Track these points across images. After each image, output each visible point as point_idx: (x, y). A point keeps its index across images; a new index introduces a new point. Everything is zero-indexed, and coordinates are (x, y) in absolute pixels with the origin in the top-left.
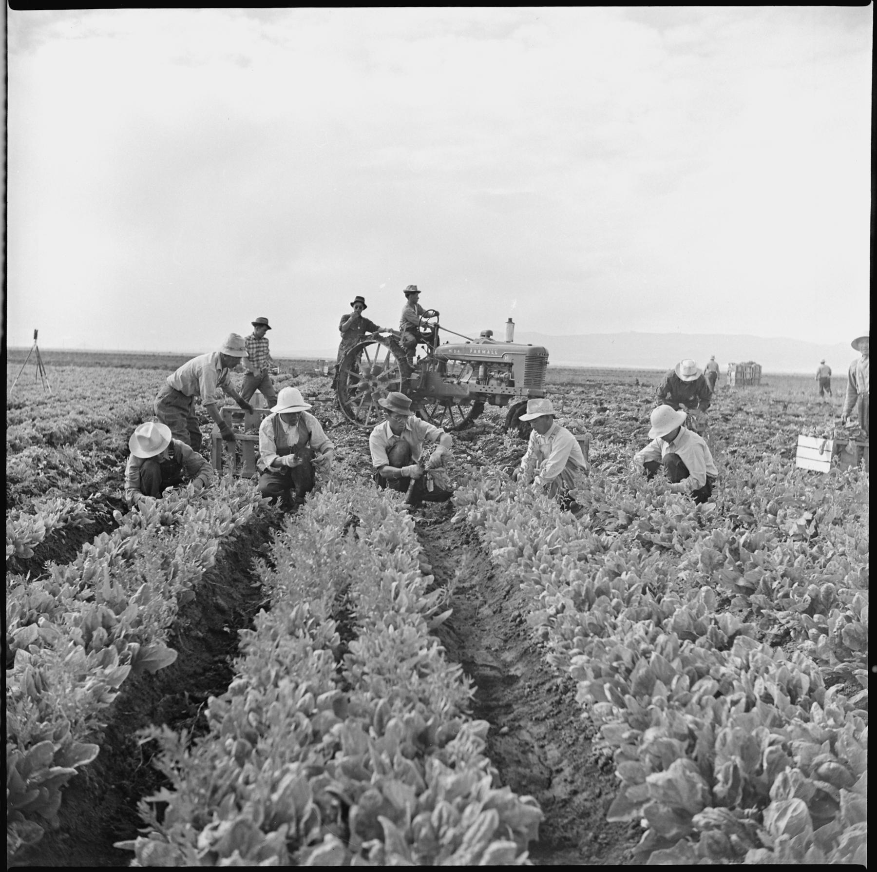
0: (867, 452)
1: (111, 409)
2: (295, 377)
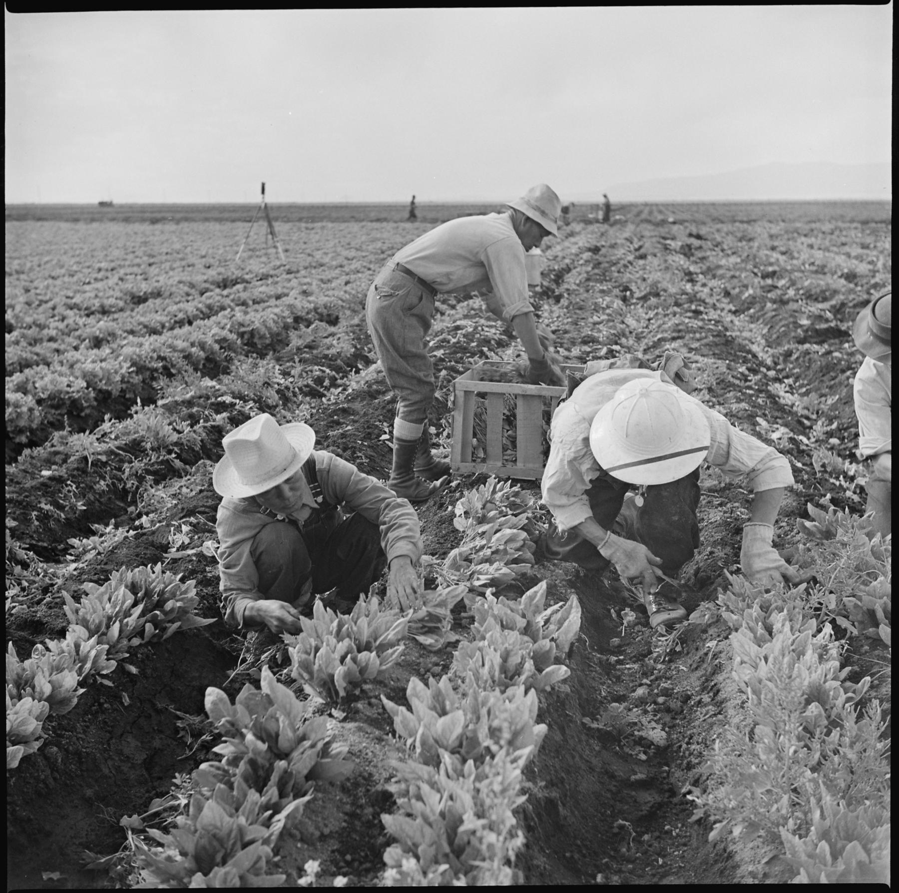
0: (877, 709)
1: (347, 283)
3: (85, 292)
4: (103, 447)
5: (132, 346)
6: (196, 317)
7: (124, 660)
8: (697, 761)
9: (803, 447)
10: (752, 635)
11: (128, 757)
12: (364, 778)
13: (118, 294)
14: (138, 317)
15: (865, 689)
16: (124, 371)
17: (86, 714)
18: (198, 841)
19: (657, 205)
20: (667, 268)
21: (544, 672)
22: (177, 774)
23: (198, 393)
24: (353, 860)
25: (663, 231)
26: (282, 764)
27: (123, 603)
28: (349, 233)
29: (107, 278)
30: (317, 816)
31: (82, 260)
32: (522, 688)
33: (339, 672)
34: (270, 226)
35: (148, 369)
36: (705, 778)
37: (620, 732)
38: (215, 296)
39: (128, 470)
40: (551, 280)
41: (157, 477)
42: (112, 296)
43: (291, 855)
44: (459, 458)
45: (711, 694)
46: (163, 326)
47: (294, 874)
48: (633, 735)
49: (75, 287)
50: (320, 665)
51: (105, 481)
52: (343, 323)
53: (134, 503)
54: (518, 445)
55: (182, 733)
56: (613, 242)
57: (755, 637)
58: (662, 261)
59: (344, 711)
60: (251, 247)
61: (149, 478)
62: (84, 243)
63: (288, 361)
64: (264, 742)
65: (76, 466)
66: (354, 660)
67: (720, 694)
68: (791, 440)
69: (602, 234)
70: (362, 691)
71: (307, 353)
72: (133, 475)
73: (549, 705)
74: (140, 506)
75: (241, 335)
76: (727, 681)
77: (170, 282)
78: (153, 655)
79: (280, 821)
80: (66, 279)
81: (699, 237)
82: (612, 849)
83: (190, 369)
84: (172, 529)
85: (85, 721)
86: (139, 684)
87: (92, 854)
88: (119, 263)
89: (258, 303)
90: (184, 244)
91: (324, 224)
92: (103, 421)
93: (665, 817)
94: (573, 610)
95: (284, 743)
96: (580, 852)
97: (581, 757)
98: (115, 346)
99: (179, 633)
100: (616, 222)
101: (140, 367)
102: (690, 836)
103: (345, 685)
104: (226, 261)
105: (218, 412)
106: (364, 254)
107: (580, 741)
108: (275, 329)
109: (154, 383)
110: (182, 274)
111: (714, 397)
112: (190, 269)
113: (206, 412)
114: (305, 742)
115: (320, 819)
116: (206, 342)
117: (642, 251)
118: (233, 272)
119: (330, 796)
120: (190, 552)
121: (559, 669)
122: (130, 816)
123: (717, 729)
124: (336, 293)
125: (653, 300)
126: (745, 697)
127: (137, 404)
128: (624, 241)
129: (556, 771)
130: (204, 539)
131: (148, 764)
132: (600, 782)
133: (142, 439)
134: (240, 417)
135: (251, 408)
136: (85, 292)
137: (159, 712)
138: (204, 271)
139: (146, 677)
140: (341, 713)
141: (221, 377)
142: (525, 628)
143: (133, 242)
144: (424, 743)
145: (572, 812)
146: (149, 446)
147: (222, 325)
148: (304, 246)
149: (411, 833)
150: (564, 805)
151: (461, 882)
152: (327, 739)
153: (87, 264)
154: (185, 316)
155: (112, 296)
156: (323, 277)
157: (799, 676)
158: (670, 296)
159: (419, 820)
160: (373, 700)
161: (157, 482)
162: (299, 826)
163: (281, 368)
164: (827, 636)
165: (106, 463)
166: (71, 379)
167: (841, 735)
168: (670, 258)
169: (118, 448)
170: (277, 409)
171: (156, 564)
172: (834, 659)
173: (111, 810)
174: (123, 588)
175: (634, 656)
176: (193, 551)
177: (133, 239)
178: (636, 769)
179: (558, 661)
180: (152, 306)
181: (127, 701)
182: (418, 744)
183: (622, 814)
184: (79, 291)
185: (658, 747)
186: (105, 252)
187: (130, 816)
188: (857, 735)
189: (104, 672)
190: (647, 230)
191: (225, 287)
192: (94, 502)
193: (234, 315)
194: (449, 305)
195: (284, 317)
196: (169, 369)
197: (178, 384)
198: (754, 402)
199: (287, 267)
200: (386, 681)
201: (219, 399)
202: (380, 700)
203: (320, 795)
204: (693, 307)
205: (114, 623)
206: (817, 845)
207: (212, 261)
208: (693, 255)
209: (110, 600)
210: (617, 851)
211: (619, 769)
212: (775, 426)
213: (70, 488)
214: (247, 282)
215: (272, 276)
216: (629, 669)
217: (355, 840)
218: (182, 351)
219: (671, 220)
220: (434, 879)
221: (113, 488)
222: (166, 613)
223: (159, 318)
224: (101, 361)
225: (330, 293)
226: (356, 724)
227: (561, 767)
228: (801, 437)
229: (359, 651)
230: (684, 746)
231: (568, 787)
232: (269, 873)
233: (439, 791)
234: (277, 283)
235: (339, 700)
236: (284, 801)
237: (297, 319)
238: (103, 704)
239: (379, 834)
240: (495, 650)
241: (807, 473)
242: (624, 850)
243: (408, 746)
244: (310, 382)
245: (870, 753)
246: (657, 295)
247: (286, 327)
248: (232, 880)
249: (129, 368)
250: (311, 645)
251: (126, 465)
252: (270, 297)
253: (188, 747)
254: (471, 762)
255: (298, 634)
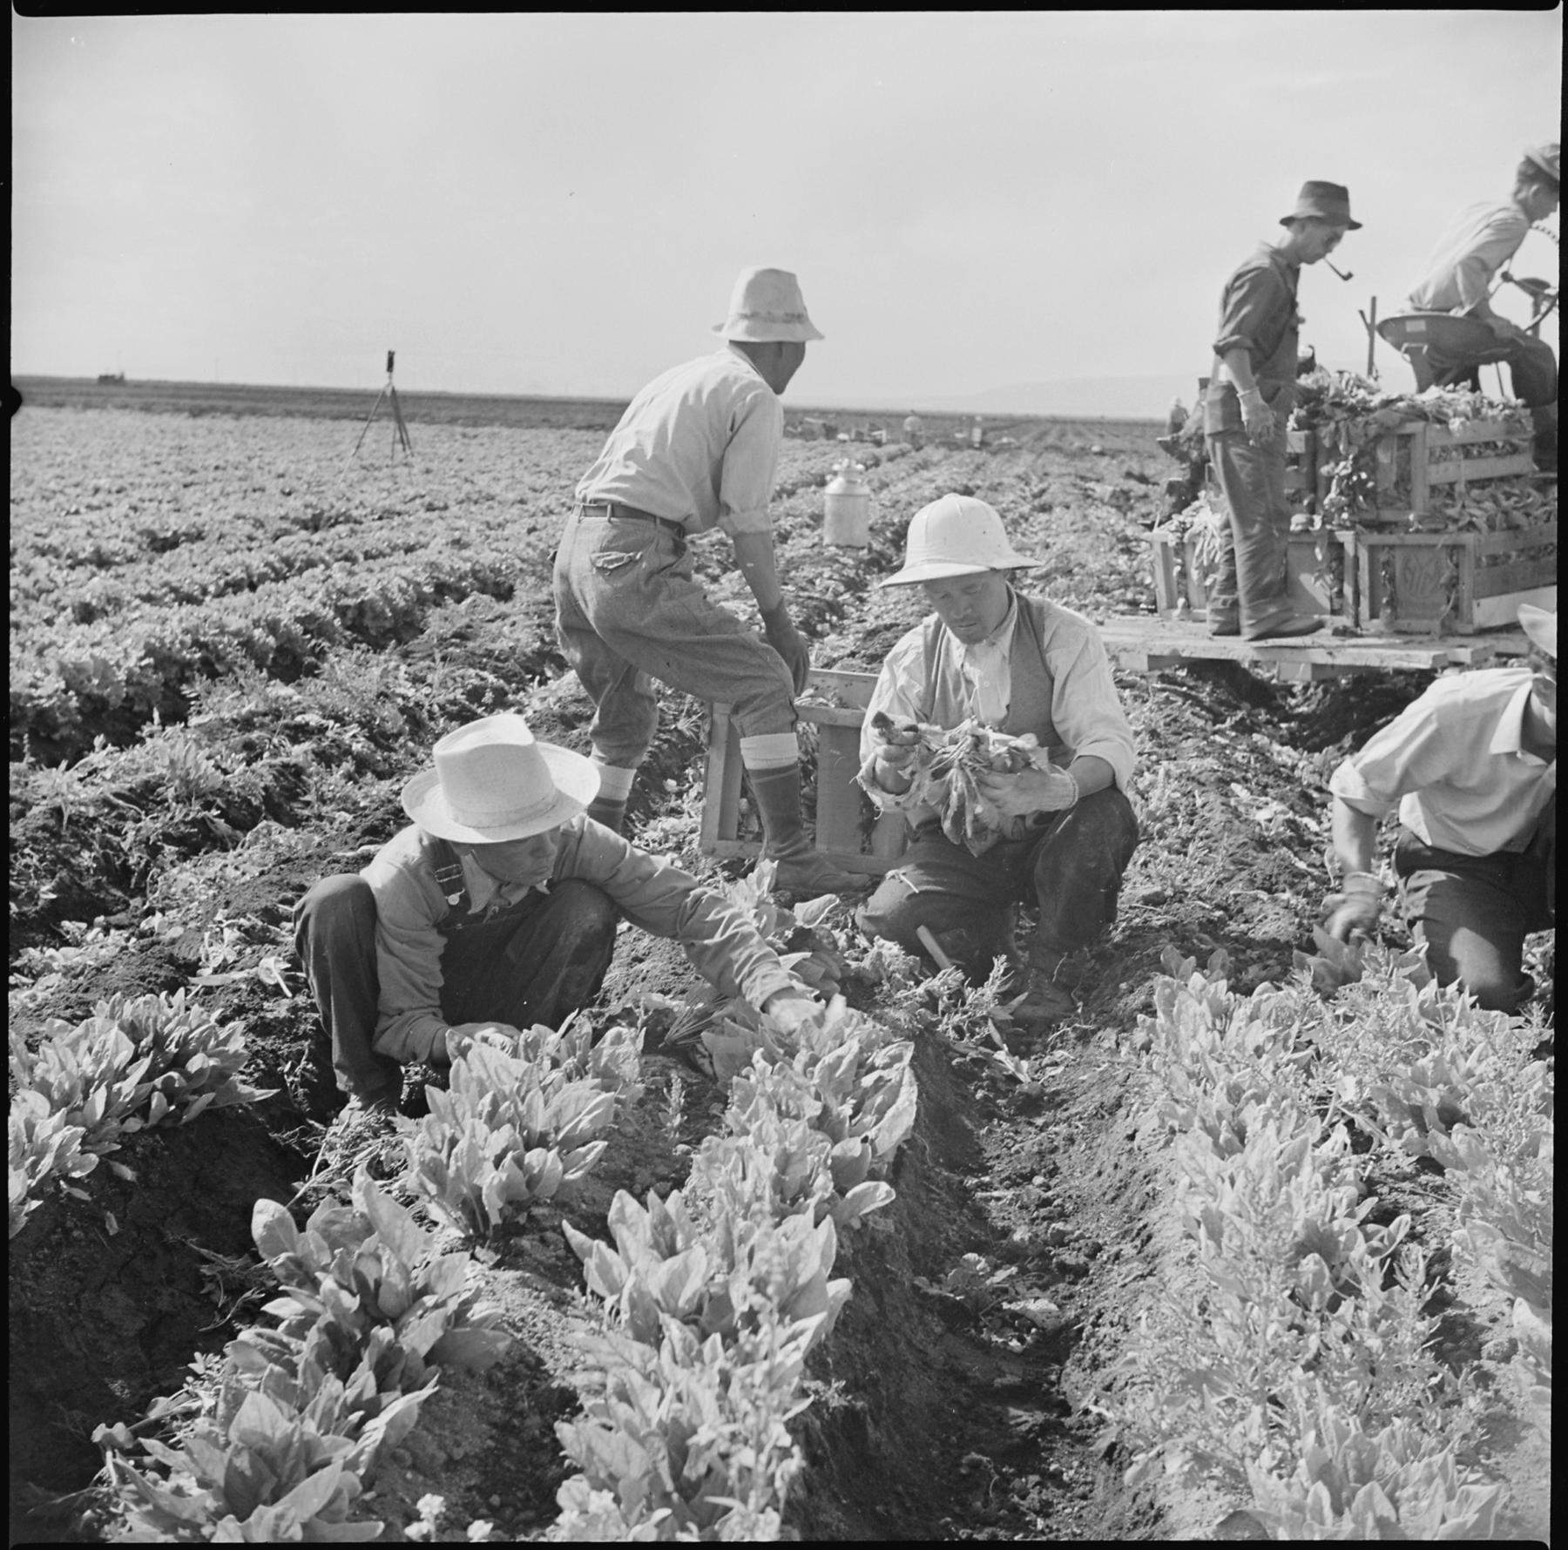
1: (531, 530)
2: (918, 450)
3: (68, 527)
4: (89, 793)
5: (150, 622)
6: (263, 578)
7: (111, 1155)
8: (1109, 1354)
9: (1308, 837)
10: (1210, 1139)
11: (111, 1325)
12: (528, 1366)
13: (129, 533)
14: (162, 572)
15: (1400, 1237)
16: (132, 663)
17: (40, 1246)
18: (230, 1461)
19: (1073, 422)
20: (1087, 529)
21: (849, 1195)
22: (197, 1355)
23: (262, 708)
24: (503, 1505)
25: (1083, 466)
26: (384, 1334)
27: (116, 1054)
28: (539, 446)
29: (109, 505)
30: (443, 1428)
31: (66, 473)
32: (810, 1214)
33: (490, 1180)
34: (402, 429)
35: (175, 662)
36: (1122, 1383)
37: (978, 1304)
38: (297, 544)
39: (131, 834)
40: (886, 540)
41: (183, 849)
42: (117, 536)
43: (394, 1491)
44: (716, 831)
45: (1138, 1242)
46: (205, 592)
47: (399, 1523)
48: (1000, 1309)
49: (50, 519)
50: (458, 1169)
51: (91, 851)
52: (522, 595)
53: (140, 891)
54: (819, 813)
55: (209, 1287)
56: (996, 481)
57: (1216, 1144)
58: (1079, 518)
59: (496, 1251)
60: (366, 463)
61: (168, 849)
62: (71, 443)
63: (423, 659)
64: (354, 1295)
65: (40, 823)
66: (519, 1161)
67: (1153, 1241)
68: (1291, 824)
69: (978, 468)
70: (531, 1218)
71: (457, 646)
72: (141, 842)
73: (856, 1252)
74: (151, 897)
75: (341, 611)
76: (1166, 1219)
77: (222, 515)
78: (164, 1149)
79: (376, 1430)
80: (37, 504)
81: (1143, 479)
82: (957, 1502)
83: (251, 666)
84: (207, 935)
85: (38, 1259)
86: (136, 1198)
87: (40, 1491)
88: (130, 479)
89: (374, 557)
90: (249, 453)
91: (496, 429)
92: (92, 748)
93: (1052, 1450)
94: (904, 1090)
95: (387, 1300)
96: (901, 1505)
97: (909, 1342)
98: (118, 620)
99: (210, 1113)
100: (1002, 449)
101: (161, 657)
102: (1093, 1483)
103: (500, 1205)
104: (319, 484)
105: (295, 741)
106: (563, 483)
107: (908, 1316)
108: (402, 604)
109: (184, 687)
110: (240, 503)
111: (1160, 746)
112: (257, 494)
113: (275, 741)
114: (426, 1299)
115: (447, 1433)
116: (279, 621)
117: (1045, 498)
118: (330, 503)
119: (469, 1395)
120: (236, 975)
121: (876, 1188)
122: (110, 1426)
123: (1144, 1300)
124: (511, 545)
125: (1061, 582)
126: (1195, 1246)
127: (152, 720)
128: (1014, 481)
129: (865, 1365)
130: (262, 953)
131: (147, 1337)
132: (942, 1389)
133: (161, 781)
134: (334, 751)
135: (354, 736)
136: (68, 527)
137: (169, 1248)
138: (282, 499)
139: (148, 1187)
140: (491, 1254)
141: (303, 680)
142: (819, 1118)
143: (159, 445)
144: (633, 1305)
145: (891, 1438)
146: (170, 793)
147: (309, 593)
148: (458, 466)
149: (606, 1456)
150: (876, 1422)
151: (691, 1536)
152: (465, 1296)
153: (75, 480)
154: (244, 575)
155: (117, 536)
156: (490, 519)
157: (1288, 1206)
158: (1092, 575)
159: (623, 1434)
160: (549, 1235)
161: (184, 857)
162: (410, 1443)
163: (411, 669)
164: (1339, 1146)
165: (95, 819)
166: (39, 674)
167: (1357, 1308)
168: (1092, 512)
169: (117, 795)
170: (402, 740)
171: (172, 992)
172: (1349, 1183)
173: (77, 1414)
174: (116, 1029)
175: (1008, 1178)
176: (243, 974)
177: (157, 441)
178: (1005, 1368)
179: (873, 1176)
180: (187, 555)
181: (113, 1226)
182: (625, 1305)
183: (975, 1443)
184: (58, 526)
185: (1042, 1331)
186: (107, 462)
187: (110, 1426)
188: (1384, 1306)
189: (76, 1174)
190: (1056, 464)
191: (316, 529)
192: (69, 887)
193: (330, 577)
194: (707, 575)
195: (418, 584)
196: (212, 665)
197: (228, 691)
198: (1226, 757)
199: (427, 499)
200: (574, 1203)
201: (299, 719)
202: (563, 1234)
203: (449, 1392)
204: (1129, 596)
205: (98, 1087)
206: (1307, 1491)
207: (295, 484)
208: (1131, 508)
209: (90, 1050)
210: (964, 1504)
211: (976, 1368)
212: (1263, 799)
213: (27, 860)
214: (356, 522)
215: (399, 514)
216: (998, 1199)
217: (509, 1470)
218: (236, 634)
219: (1096, 449)
220: (646, 1532)
221: (105, 866)
222: (188, 1077)
223: (197, 577)
224: (93, 645)
225: (502, 545)
226: (519, 1273)
227: (874, 1359)
228: (1306, 820)
229: (528, 1148)
230: (1088, 1329)
231: (884, 1393)
232: (353, 1518)
233: (657, 1384)
234: (408, 524)
235: (490, 1233)
236: (386, 1398)
237: (442, 589)
238: (71, 1230)
239: (551, 1462)
240: (766, 1153)
241: (1314, 878)
242: (979, 1504)
243: (607, 1309)
244: (461, 698)
245: (1405, 1338)
246: (1069, 573)
247: (422, 600)
248: (288, 1528)
249: (141, 659)
250: (444, 1136)
251: (129, 825)
252: (394, 548)
253: (220, 1311)
254: (716, 1337)
255: (422, 1116)
